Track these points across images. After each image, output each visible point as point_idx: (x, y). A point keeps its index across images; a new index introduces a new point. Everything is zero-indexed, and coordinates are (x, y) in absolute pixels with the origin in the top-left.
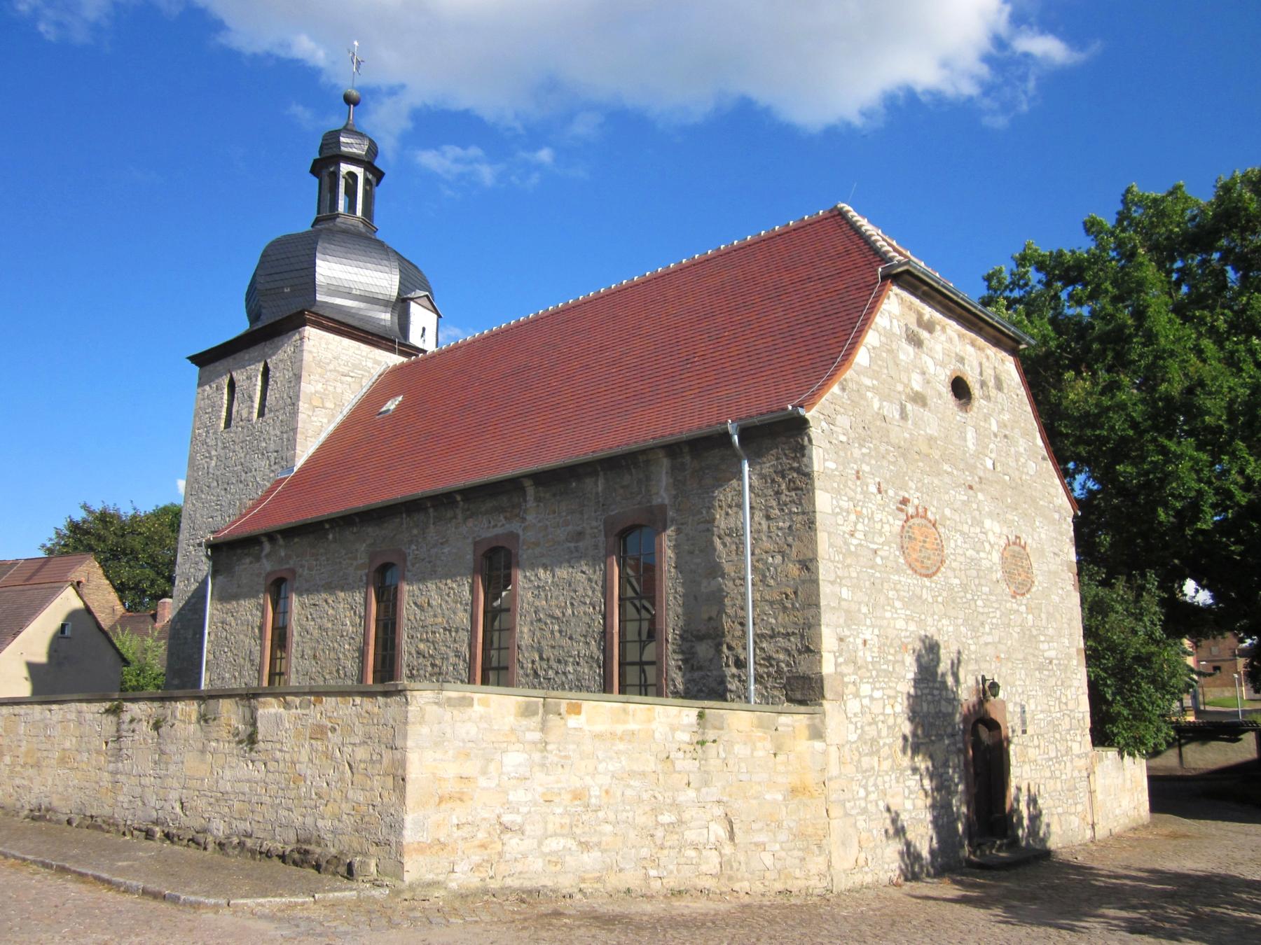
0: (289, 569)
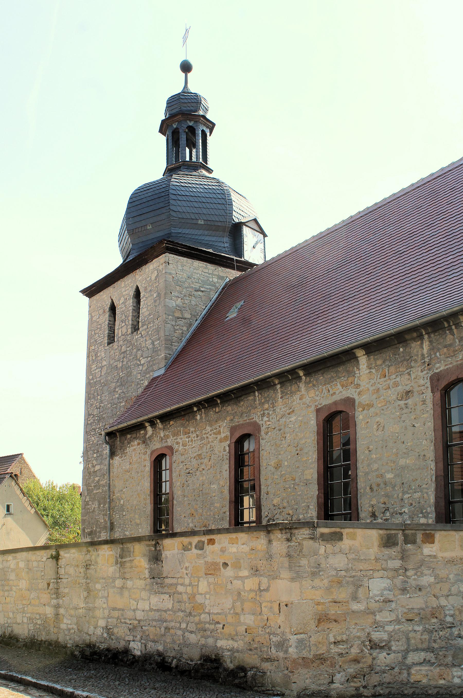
0: (166, 447)
